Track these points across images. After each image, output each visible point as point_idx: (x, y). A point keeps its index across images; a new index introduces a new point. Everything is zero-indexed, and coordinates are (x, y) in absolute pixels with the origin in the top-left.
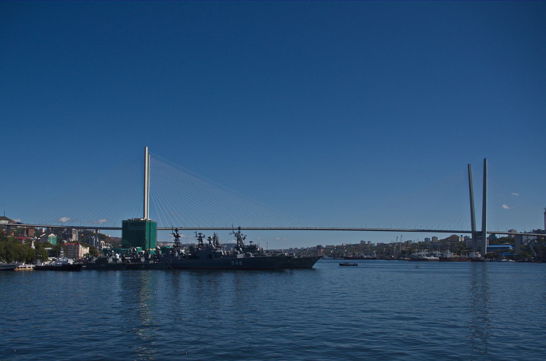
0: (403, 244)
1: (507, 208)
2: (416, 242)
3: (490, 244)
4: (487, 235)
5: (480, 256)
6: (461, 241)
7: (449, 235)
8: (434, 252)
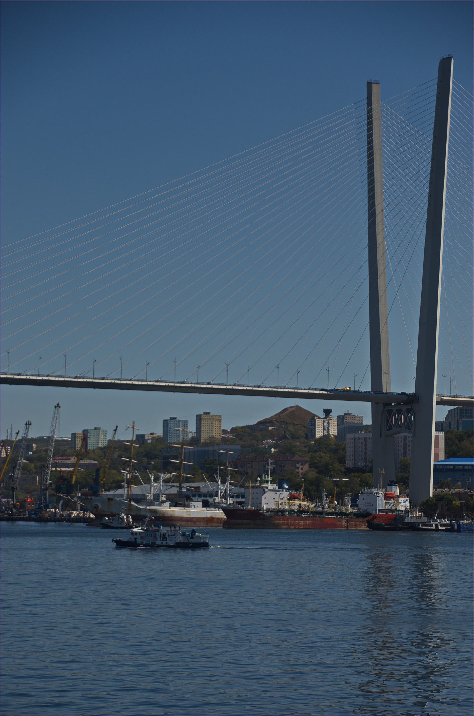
0: (63, 448)
1: (470, 521)
2: (126, 436)
3: (449, 454)
4: (439, 414)
5: (404, 504)
6: (326, 437)
7: (273, 407)
8: (206, 486)
